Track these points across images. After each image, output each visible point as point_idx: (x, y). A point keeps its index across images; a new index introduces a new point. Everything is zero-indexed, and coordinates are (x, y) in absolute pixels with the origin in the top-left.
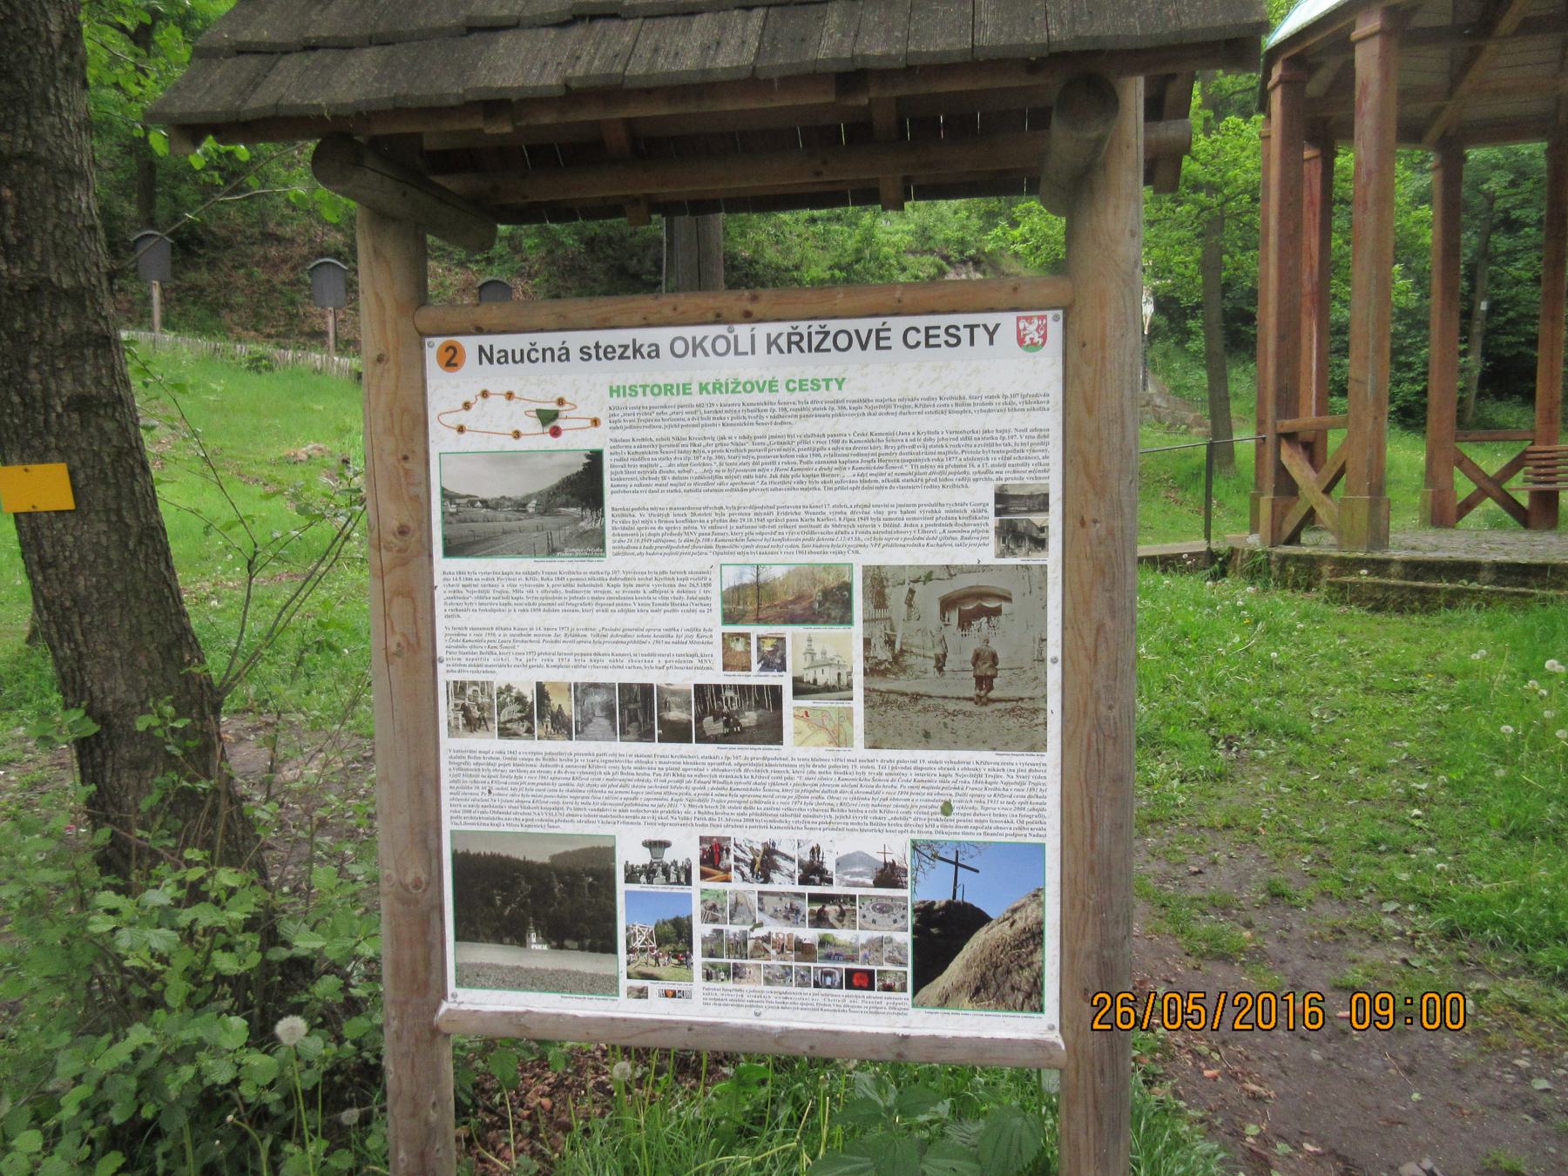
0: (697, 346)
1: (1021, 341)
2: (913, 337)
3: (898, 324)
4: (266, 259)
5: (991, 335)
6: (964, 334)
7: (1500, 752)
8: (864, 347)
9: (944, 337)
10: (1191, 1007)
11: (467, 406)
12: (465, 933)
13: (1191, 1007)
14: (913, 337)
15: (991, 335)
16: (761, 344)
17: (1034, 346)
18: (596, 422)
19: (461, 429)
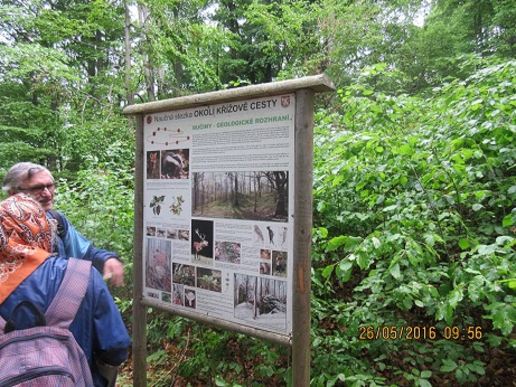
0: (200, 113)
1: (282, 105)
2: (253, 106)
3: (249, 103)
4: (325, 136)
5: (274, 103)
6: (267, 104)
7: (158, 283)
8: (240, 110)
9: (261, 105)
10: (392, 332)
11: (154, 134)
12: (148, 285)
13: (392, 332)
14: (253, 106)
15: (274, 103)
16: (216, 111)
17: (286, 106)
18: (188, 138)
19: (153, 142)
